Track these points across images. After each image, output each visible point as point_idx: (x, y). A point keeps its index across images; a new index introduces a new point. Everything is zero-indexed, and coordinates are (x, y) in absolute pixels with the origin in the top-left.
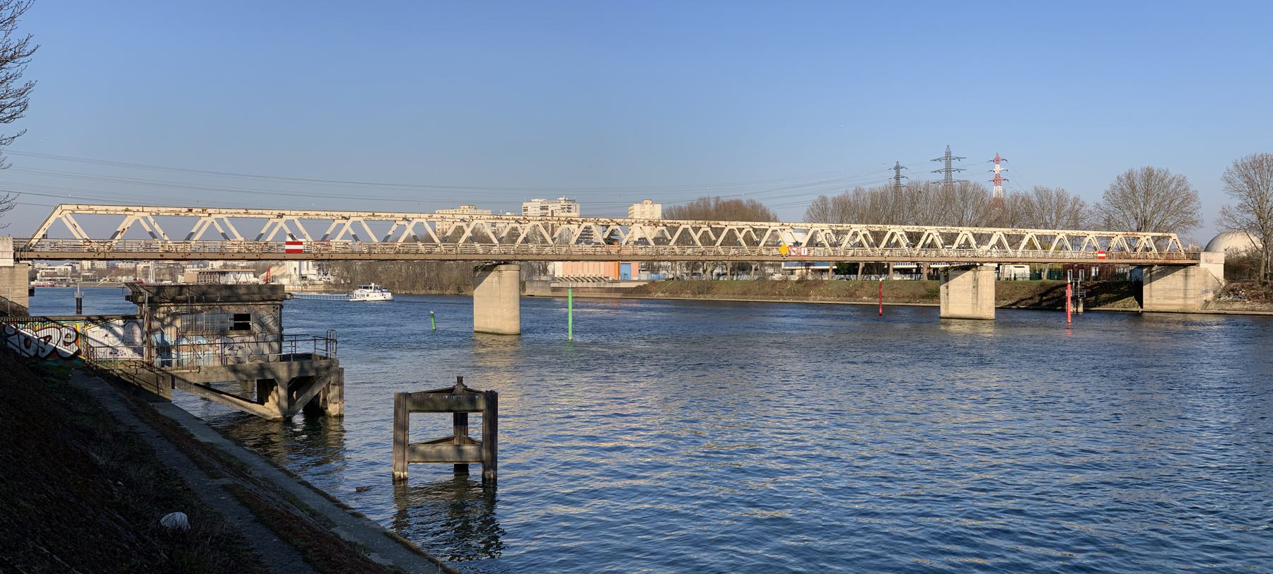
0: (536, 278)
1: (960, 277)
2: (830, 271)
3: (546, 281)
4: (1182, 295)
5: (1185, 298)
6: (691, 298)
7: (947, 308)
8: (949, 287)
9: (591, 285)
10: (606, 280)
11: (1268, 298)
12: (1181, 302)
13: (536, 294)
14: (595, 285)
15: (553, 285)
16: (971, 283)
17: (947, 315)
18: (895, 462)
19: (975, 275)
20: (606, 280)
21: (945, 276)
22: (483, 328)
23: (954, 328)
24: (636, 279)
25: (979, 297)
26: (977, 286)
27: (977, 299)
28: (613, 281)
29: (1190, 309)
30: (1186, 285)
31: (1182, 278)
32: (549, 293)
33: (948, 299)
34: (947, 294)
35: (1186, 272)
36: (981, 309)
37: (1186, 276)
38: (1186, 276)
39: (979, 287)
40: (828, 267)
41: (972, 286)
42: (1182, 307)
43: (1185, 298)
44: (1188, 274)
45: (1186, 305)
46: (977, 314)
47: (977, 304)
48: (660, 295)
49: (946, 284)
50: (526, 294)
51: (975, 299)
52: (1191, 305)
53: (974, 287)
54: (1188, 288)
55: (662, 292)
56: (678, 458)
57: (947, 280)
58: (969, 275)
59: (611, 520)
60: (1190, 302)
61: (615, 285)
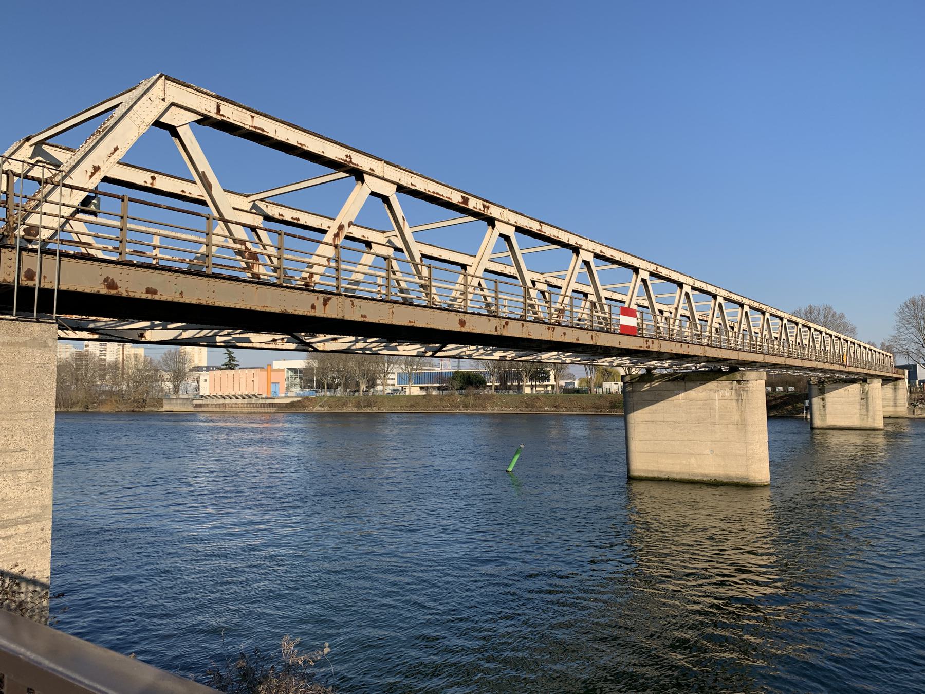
0: (292, 389)
3: (187, 399)
5: (895, 405)
6: (355, 410)
7: (824, 417)
8: (826, 400)
9: (240, 401)
10: (259, 397)
12: (891, 409)
13: (174, 409)
14: (245, 401)
15: (195, 402)
17: (824, 426)
18: (128, 434)
20: (259, 397)
21: (820, 389)
23: (836, 439)
24: (283, 395)
25: (871, 408)
27: (867, 410)
28: (267, 398)
29: (900, 414)
30: (895, 396)
32: (192, 409)
36: (874, 419)
37: (895, 389)
38: (895, 388)
40: (491, 384)
42: (892, 413)
45: (896, 412)
46: (869, 424)
47: (867, 415)
48: (318, 409)
50: (163, 409)
51: (864, 412)
52: (902, 412)
54: (898, 398)
55: (321, 406)
56: (264, 476)
59: (846, 668)
60: (899, 409)
61: (268, 401)
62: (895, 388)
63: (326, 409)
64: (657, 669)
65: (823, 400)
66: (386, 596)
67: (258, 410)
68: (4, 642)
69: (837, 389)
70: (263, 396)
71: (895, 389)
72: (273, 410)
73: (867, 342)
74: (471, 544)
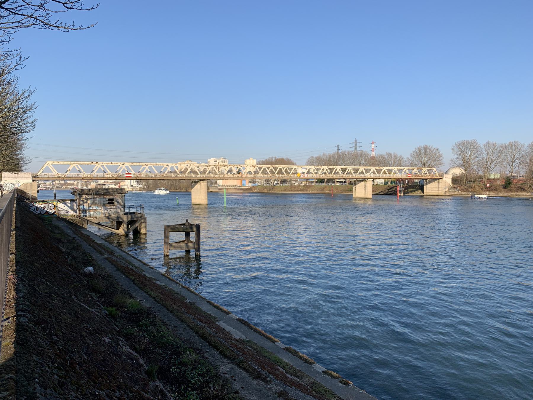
7: (355, 195)
9: (232, 188)
12: (437, 192)
14: (234, 188)
15: (219, 188)
17: (356, 197)
28: (240, 186)
30: (439, 186)
32: (218, 191)
37: (439, 183)
38: (439, 183)
45: (438, 193)
48: (256, 191)
61: (240, 188)
62: (439, 183)
63: (258, 191)
64: (419, 371)
65: (355, 187)
66: (300, 283)
67: (237, 191)
68: (532, 399)
69: (359, 183)
70: (239, 185)
71: (439, 183)
72: (242, 191)
73: (409, 164)
74: (329, 255)
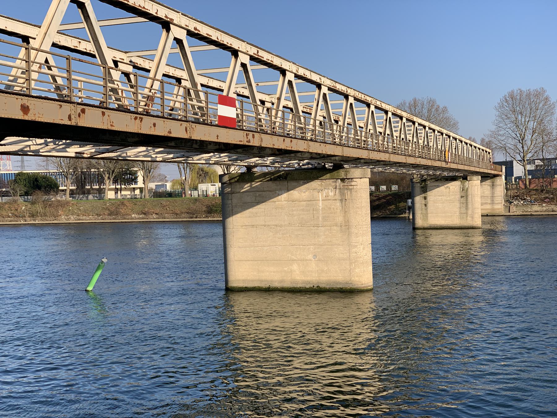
1: (443, 187)
2: (68, 192)
4: (489, 201)
5: (493, 203)
7: (426, 216)
8: (428, 198)
11: (551, 201)
16: (459, 194)
17: (426, 225)
19: (463, 185)
21: (422, 187)
22: (244, 281)
25: (470, 206)
26: (467, 196)
27: (467, 208)
30: (493, 193)
31: (489, 187)
33: (426, 209)
34: (426, 205)
35: (493, 182)
37: (493, 186)
38: (493, 185)
39: (470, 197)
40: (65, 188)
41: (459, 196)
42: (489, 211)
43: (493, 203)
44: (495, 183)
45: (493, 209)
47: (467, 213)
49: (423, 195)
51: (463, 210)
52: (499, 209)
53: (462, 197)
54: (495, 195)
57: (424, 190)
58: (455, 186)
